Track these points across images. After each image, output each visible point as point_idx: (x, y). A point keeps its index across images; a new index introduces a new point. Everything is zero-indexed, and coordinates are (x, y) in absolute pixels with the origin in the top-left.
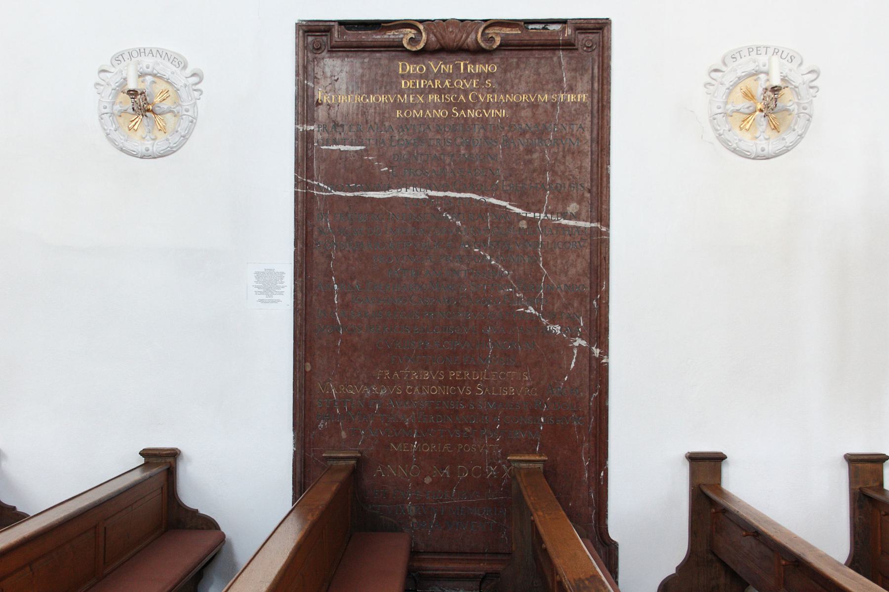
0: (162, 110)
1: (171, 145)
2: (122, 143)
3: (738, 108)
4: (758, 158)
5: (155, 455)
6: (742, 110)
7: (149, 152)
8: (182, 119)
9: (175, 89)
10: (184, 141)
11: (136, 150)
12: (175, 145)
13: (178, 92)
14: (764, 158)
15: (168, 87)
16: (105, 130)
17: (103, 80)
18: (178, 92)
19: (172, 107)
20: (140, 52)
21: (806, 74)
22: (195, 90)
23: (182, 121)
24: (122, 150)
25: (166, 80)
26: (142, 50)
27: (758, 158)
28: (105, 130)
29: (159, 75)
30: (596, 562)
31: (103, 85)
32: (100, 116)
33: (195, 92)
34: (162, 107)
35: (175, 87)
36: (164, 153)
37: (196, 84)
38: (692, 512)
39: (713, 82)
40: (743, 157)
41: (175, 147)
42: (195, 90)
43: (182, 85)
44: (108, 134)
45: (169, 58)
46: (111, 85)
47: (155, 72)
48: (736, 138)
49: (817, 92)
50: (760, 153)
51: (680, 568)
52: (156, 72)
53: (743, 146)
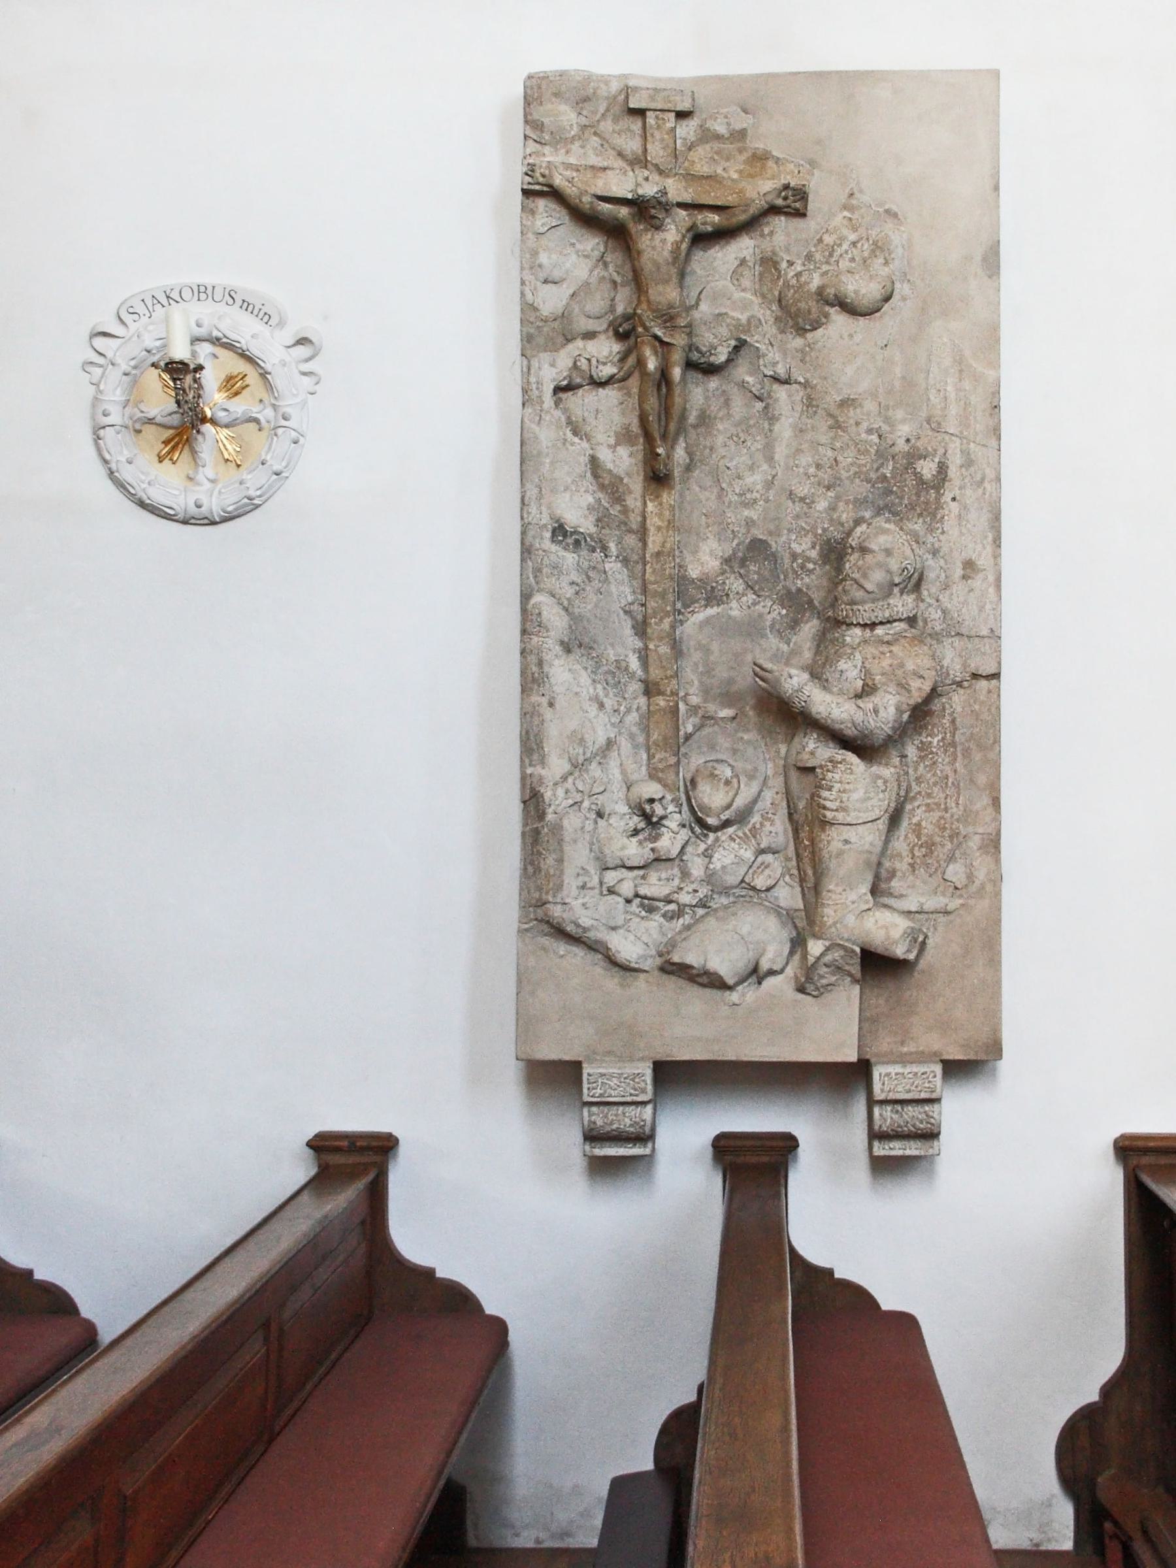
0: (234, 416)
1: (252, 493)
2: (144, 490)
3: (150, 415)
4: (193, 521)
5: (1146, 1151)
6: (159, 419)
7: (204, 510)
8: (276, 435)
9: (262, 371)
10: (279, 484)
11: (175, 506)
12: (259, 493)
13: (268, 376)
14: (206, 521)
15: (241, 366)
16: (106, 462)
17: (101, 354)
18: (268, 376)
19: (255, 410)
20: (202, 292)
21: (95, 350)
22: (304, 374)
23: (275, 438)
24: (142, 504)
25: (240, 351)
26: (202, 289)
27: (193, 521)
28: (106, 462)
29: (225, 340)
30: (695, 1449)
31: (101, 366)
32: (94, 433)
33: (303, 377)
34: (231, 410)
35: (262, 368)
36: (236, 509)
37: (308, 360)
38: (158, 1381)
39: (101, 360)
40: (163, 517)
41: (260, 496)
42: (304, 374)
43: (276, 361)
44: (111, 473)
45: (171, 301)
46: (119, 365)
47: (215, 333)
48: (143, 477)
49: (317, 383)
50: (193, 510)
51: (1108, 1390)
52: (220, 335)
53: (157, 496)
